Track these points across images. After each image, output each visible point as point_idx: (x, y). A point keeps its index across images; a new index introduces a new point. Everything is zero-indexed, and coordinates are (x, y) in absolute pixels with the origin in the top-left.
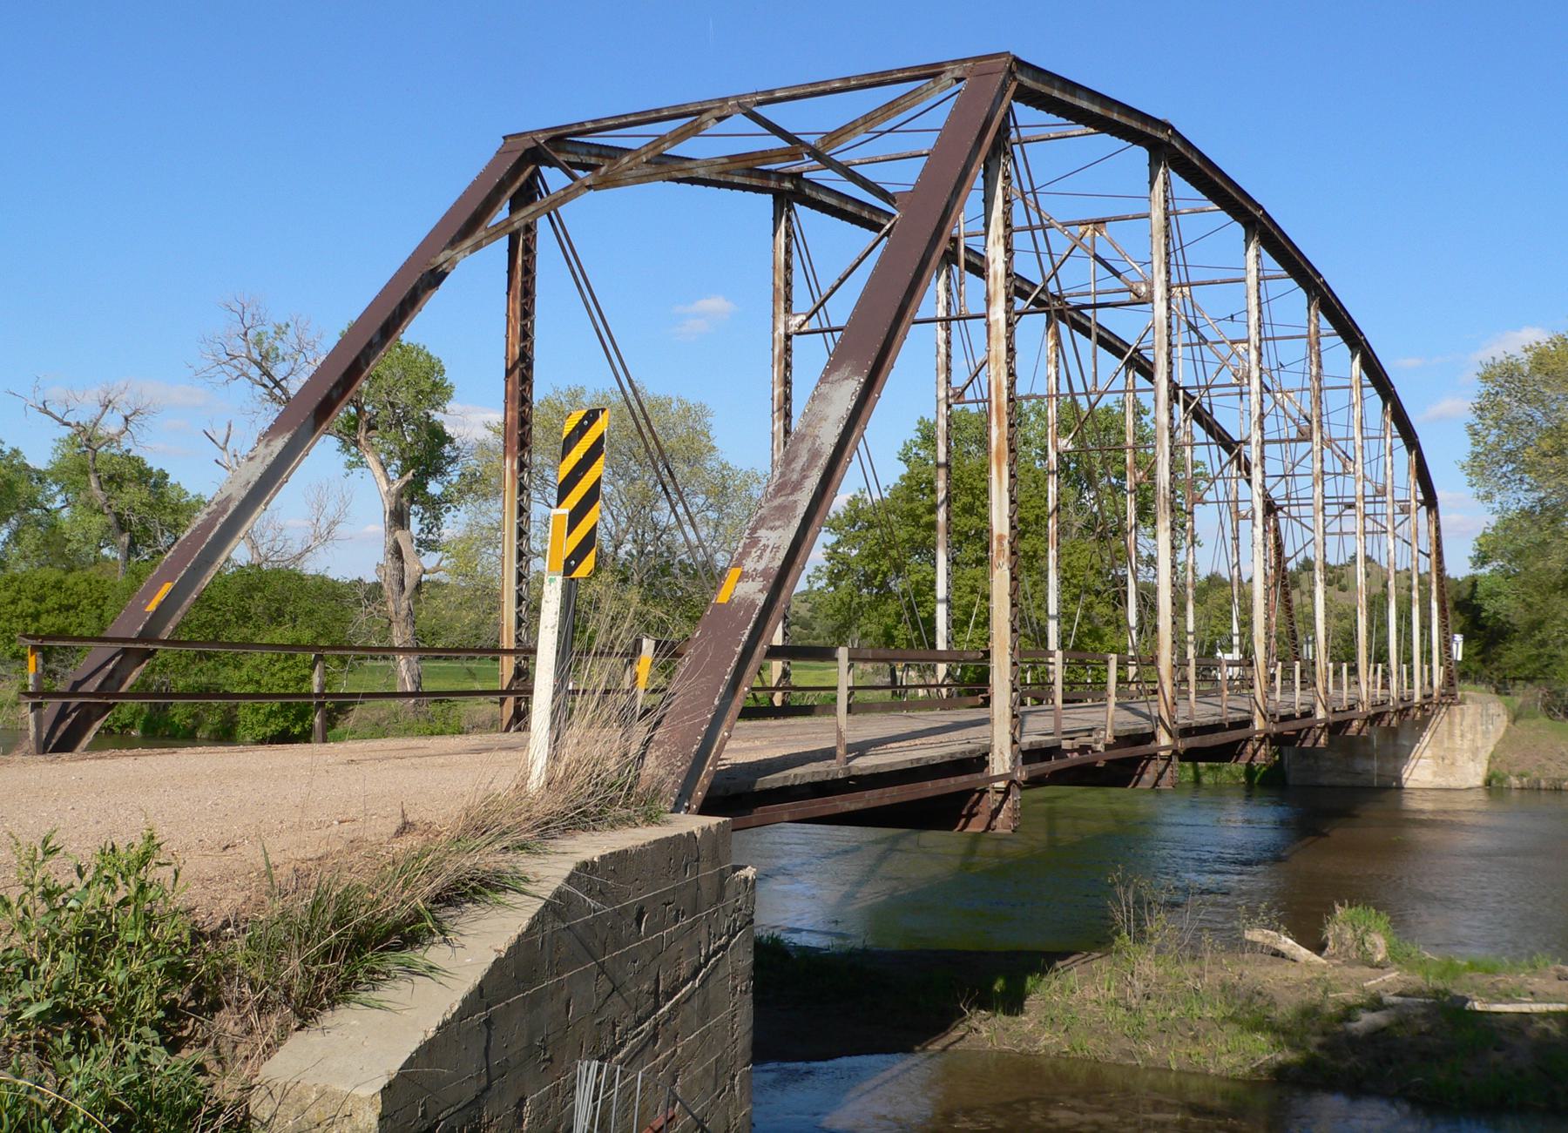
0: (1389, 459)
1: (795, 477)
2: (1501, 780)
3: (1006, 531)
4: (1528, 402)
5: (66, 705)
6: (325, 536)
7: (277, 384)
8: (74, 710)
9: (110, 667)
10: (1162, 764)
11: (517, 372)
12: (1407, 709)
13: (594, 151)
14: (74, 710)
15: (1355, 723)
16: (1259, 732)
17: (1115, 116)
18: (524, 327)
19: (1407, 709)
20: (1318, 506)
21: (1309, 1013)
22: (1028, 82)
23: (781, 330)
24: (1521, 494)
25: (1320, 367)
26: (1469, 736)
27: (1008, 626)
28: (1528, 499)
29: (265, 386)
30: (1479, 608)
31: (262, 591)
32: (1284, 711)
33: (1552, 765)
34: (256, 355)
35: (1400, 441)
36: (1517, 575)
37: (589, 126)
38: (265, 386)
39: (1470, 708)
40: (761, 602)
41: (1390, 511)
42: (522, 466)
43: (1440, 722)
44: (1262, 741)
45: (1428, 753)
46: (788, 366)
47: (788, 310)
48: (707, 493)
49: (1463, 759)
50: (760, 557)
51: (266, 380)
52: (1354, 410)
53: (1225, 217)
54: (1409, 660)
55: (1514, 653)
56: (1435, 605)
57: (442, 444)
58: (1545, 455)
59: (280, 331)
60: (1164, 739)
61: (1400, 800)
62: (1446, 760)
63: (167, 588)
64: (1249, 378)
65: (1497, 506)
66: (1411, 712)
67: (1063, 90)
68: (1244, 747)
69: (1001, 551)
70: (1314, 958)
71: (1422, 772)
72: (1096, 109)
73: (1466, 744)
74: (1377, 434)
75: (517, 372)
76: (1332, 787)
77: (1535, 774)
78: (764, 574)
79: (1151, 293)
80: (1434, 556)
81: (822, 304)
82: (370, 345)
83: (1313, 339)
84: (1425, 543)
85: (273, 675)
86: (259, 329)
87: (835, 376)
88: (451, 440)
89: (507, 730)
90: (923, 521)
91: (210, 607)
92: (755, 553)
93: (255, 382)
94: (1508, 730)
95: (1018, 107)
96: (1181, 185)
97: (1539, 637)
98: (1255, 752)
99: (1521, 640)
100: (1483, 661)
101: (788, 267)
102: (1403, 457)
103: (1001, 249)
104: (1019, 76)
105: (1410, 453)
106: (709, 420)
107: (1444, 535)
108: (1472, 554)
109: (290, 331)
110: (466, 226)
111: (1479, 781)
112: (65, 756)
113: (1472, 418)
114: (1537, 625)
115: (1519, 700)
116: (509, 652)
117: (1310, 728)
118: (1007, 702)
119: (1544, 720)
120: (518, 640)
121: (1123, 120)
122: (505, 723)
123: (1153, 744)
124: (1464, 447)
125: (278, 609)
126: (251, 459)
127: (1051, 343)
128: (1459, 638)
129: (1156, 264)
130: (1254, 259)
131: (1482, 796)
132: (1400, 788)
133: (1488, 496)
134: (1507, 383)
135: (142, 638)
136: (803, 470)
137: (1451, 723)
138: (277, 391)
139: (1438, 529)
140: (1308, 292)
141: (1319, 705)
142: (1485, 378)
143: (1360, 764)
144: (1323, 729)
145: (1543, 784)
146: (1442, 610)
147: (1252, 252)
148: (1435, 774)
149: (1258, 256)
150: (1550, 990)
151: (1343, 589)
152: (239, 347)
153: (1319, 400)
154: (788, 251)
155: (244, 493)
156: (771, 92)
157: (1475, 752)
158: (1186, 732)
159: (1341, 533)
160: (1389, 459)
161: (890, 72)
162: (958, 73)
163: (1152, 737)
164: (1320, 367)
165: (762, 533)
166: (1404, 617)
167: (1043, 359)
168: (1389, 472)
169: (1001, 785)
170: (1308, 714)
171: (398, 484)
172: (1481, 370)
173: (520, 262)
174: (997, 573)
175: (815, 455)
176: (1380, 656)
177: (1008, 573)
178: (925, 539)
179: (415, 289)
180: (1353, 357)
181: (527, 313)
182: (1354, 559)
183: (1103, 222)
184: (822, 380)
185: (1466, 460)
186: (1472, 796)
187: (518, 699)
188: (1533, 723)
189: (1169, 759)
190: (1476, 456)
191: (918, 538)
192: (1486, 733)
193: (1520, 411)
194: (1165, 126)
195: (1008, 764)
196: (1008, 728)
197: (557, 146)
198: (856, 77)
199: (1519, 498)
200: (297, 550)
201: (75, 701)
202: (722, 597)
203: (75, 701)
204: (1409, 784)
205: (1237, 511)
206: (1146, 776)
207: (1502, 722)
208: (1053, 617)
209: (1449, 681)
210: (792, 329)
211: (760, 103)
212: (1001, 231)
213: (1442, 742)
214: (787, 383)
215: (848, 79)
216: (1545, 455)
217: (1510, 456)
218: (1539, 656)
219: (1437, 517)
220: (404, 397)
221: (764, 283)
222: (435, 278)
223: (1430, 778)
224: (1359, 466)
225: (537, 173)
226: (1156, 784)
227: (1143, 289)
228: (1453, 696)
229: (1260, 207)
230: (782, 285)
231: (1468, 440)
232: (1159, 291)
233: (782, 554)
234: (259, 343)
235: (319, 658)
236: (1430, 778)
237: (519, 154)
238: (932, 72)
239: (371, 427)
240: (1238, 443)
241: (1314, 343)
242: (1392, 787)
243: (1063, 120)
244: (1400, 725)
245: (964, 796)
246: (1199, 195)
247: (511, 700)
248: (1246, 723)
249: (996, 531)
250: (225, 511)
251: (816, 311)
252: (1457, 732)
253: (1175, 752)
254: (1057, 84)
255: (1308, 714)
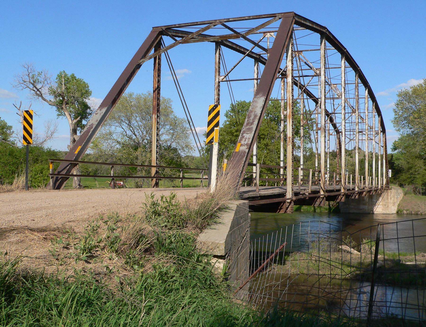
0: (374, 119)
1: (251, 121)
2: (401, 212)
3: (291, 136)
4: (411, 103)
5: (57, 178)
6: (50, 137)
7: (38, 90)
8: (60, 179)
9: (68, 168)
10: (321, 199)
11: (156, 91)
12: (377, 190)
13: (175, 31)
14: (60, 179)
15: (364, 193)
16: (342, 193)
17: (314, 27)
18: (158, 79)
19: (377, 190)
20: (350, 131)
21: (361, 264)
22: (297, 19)
23: (217, 80)
24: (408, 130)
25: (358, 93)
26: (393, 199)
27: (291, 160)
28: (409, 131)
29: (34, 91)
30: (393, 163)
31: (32, 153)
32: (348, 188)
33: (415, 207)
34: (32, 81)
35: (376, 114)
36: (405, 153)
37: (177, 26)
38: (34, 91)
39: (393, 191)
40: (247, 152)
41: (374, 133)
42: (158, 116)
43: (384, 195)
44: (343, 195)
45: (381, 203)
46: (219, 90)
47: (219, 75)
48: (171, 125)
49: (390, 205)
50: (245, 140)
51: (34, 89)
52: (366, 105)
53: (336, 51)
54: (377, 176)
55: (404, 176)
56: (384, 161)
57: (87, 109)
58: (415, 118)
59: (40, 74)
60: (322, 193)
61: (373, 217)
62: (386, 206)
63: (80, 148)
64: (341, 96)
65: (401, 133)
66: (378, 191)
67: (304, 21)
68: (338, 197)
69: (289, 141)
70: (358, 253)
71: (379, 209)
72: (311, 25)
73: (392, 201)
74: (371, 111)
75: (156, 91)
76: (353, 213)
77: (411, 210)
78: (247, 144)
79: (320, 73)
80: (384, 147)
81: (227, 75)
82: (124, 84)
83: (357, 85)
84: (382, 144)
85: (35, 179)
86: (33, 73)
87: (258, 96)
88: (89, 108)
89: (154, 187)
90: (234, 134)
91: (16, 158)
92: (244, 140)
93: (31, 89)
94: (403, 197)
95: (295, 26)
96: (328, 44)
97: (411, 172)
98: (341, 198)
99: (405, 173)
100: (394, 179)
101: (219, 63)
102: (377, 118)
103: (290, 63)
104: (295, 18)
105: (379, 117)
106: (171, 103)
107: (387, 142)
108: (392, 147)
109: (43, 74)
110: (143, 54)
111: (395, 212)
112: (58, 190)
113: (395, 107)
114: (410, 168)
115: (407, 189)
116: (154, 166)
117: (354, 193)
118: (291, 180)
119: (413, 195)
120: (157, 163)
121: (316, 27)
122: (153, 186)
123: (319, 194)
124: (392, 116)
125: (36, 159)
126: (96, 114)
127: (282, 84)
128: (390, 171)
129: (322, 65)
130: (343, 63)
131: (395, 215)
132: (373, 213)
133: (399, 130)
134: (405, 97)
135: (75, 160)
136: (253, 119)
137: (388, 195)
138: (38, 92)
139: (386, 139)
140: (355, 72)
141: (356, 187)
142: (399, 95)
143: (362, 207)
144: (357, 193)
145: (413, 213)
146: (386, 162)
147: (343, 61)
148: (383, 210)
149: (345, 62)
150: (420, 259)
151: (352, 157)
152: (27, 79)
153: (358, 102)
154: (219, 59)
155: (97, 123)
156: (229, 19)
157: (394, 204)
158: (327, 191)
159: (362, 140)
160: (374, 119)
161: (262, 15)
162: (280, 17)
163: (319, 192)
164: (358, 93)
165: (244, 135)
166: (371, 166)
167: (280, 88)
168: (374, 123)
169: (289, 201)
170: (353, 189)
171: (75, 121)
172: (398, 94)
173: (157, 62)
174: (288, 147)
175: (255, 116)
176: (371, 175)
177: (291, 147)
178: (235, 140)
179: (134, 69)
180: (366, 90)
181: (159, 76)
182: (355, 148)
183: (302, 51)
184: (255, 97)
185: (393, 119)
186: (393, 216)
187: (156, 179)
188: (410, 196)
189: (323, 198)
190: (396, 118)
191: (233, 139)
192: (397, 198)
193: (408, 105)
194: (325, 28)
195: (291, 196)
196: (291, 186)
197: (167, 31)
198: (252, 16)
199: (407, 131)
200: (41, 141)
201: (60, 177)
202: (237, 150)
203: (60, 177)
204: (375, 212)
205: (329, 133)
206: (317, 203)
207: (402, 195)
208: (282, 161)
209: (387, 183)
210: (220, 80)
211: (225, 22)
212: (290, 58)
213: (385, 200)
214: (219, 95)
215: (250, 17)
216: (415, 118)
217: (405, 118)
218: (411, 177)
219: (386, 136)
220: (77, 95)
221: (213, 67)
222: (139, 66)
223: (381, 211)
224: (367, 121)
225: (161, 38)
226: (320, 205)
227: (318, 72)
228: (388, 187)
229: (346, 49)
230: (218, 68)
231: (394, 114)
232: (322, 73)
233: (251, 140)
234: (33, 77)
235: (113, 167)
236: (381, 211)
237: (158, 33)
238: (273, 16)
239: (67, 104)
240: (330, 114)
241: (357, 87)
242: (371, 213)
243: (297, 26)
244: (374, 195)
245: (279, 204)
246: (331, 45)
247: (155, 179)
248: (339, 190)
249: (288, 136)
250: (92, 128)
251: (226, 77)
252: (389, 198)
253: (325, 196)
254: (303, 19)
255: (353, 189)
